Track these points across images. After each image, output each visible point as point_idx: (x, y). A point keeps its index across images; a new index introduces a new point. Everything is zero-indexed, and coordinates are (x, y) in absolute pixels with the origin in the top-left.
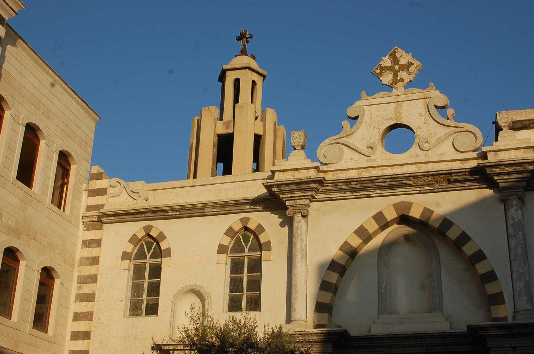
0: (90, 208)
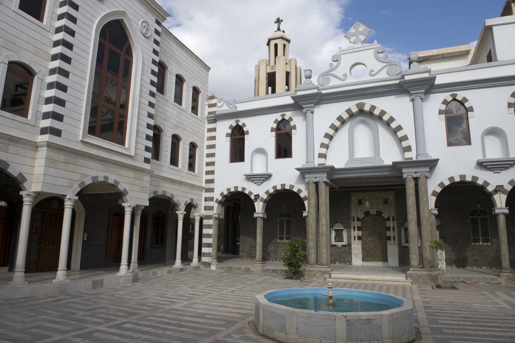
0: (209, 113)
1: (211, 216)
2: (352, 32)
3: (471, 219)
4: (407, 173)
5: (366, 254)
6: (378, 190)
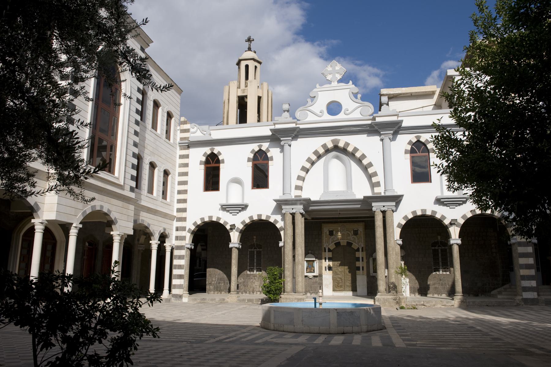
0: (182, 139)
1: (183, 246)
2: (329, 70)
3: (433, 250)
4: (377, 206)
5: (336, 284)
6: (349, 222)
